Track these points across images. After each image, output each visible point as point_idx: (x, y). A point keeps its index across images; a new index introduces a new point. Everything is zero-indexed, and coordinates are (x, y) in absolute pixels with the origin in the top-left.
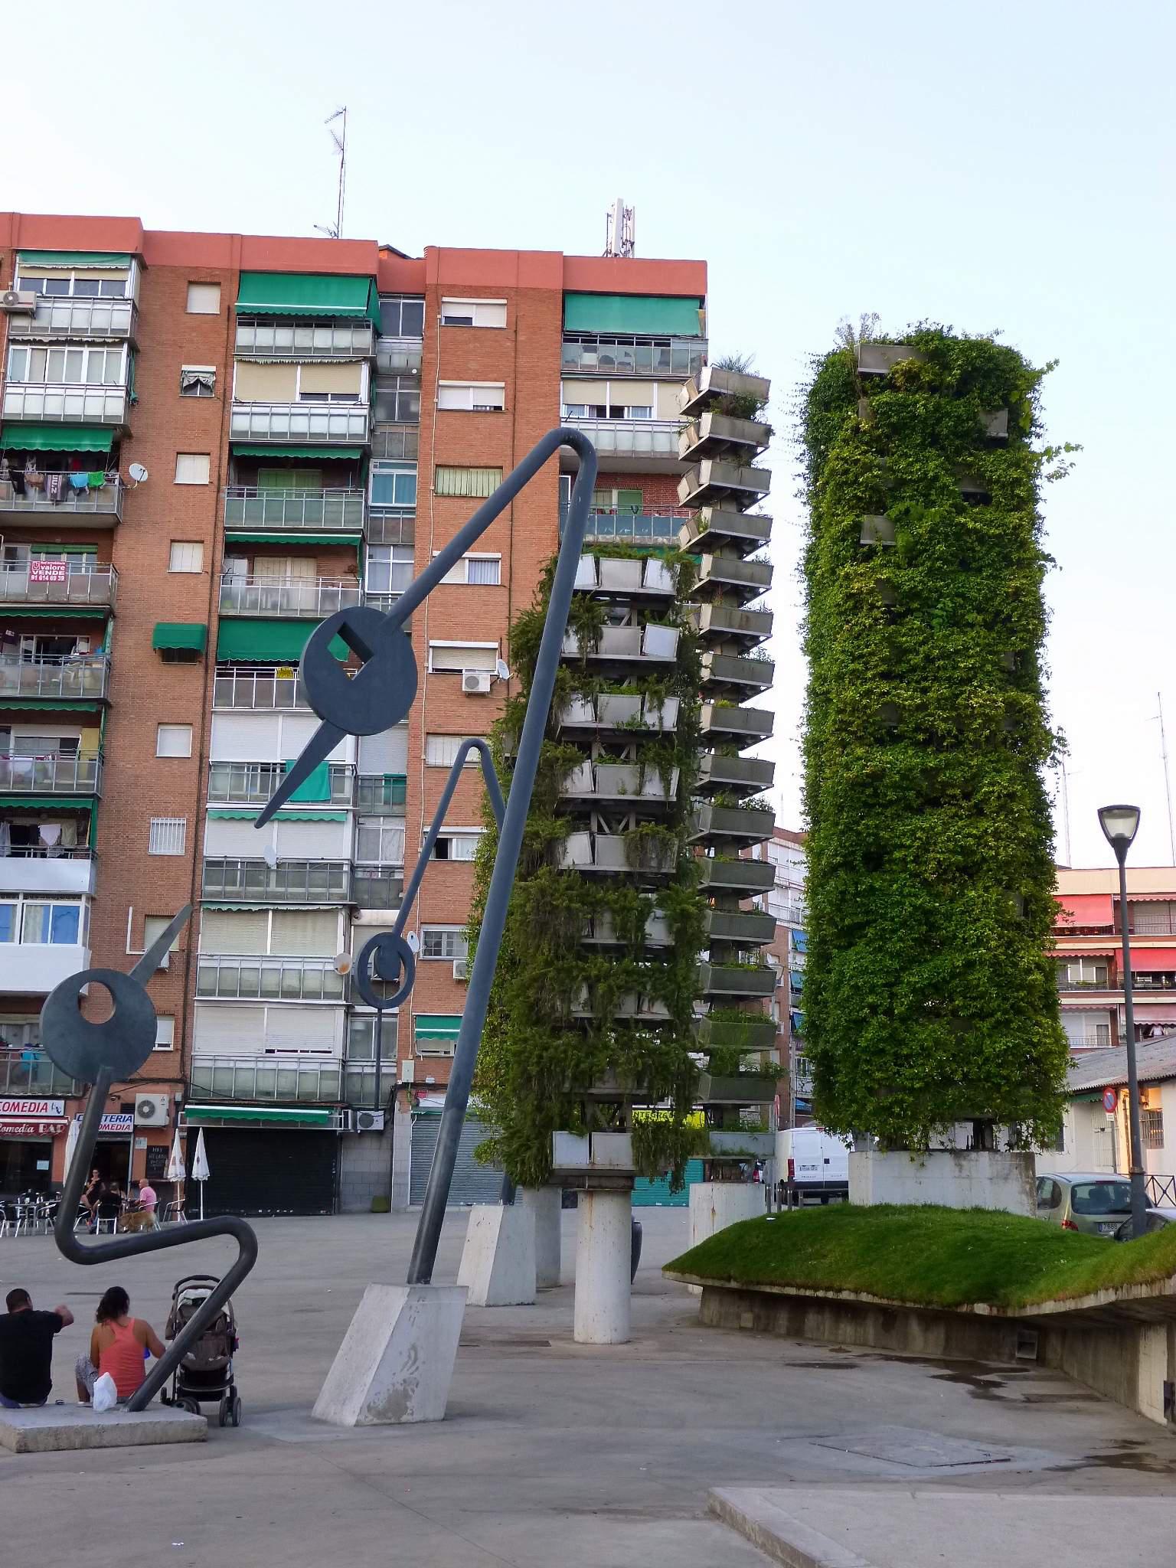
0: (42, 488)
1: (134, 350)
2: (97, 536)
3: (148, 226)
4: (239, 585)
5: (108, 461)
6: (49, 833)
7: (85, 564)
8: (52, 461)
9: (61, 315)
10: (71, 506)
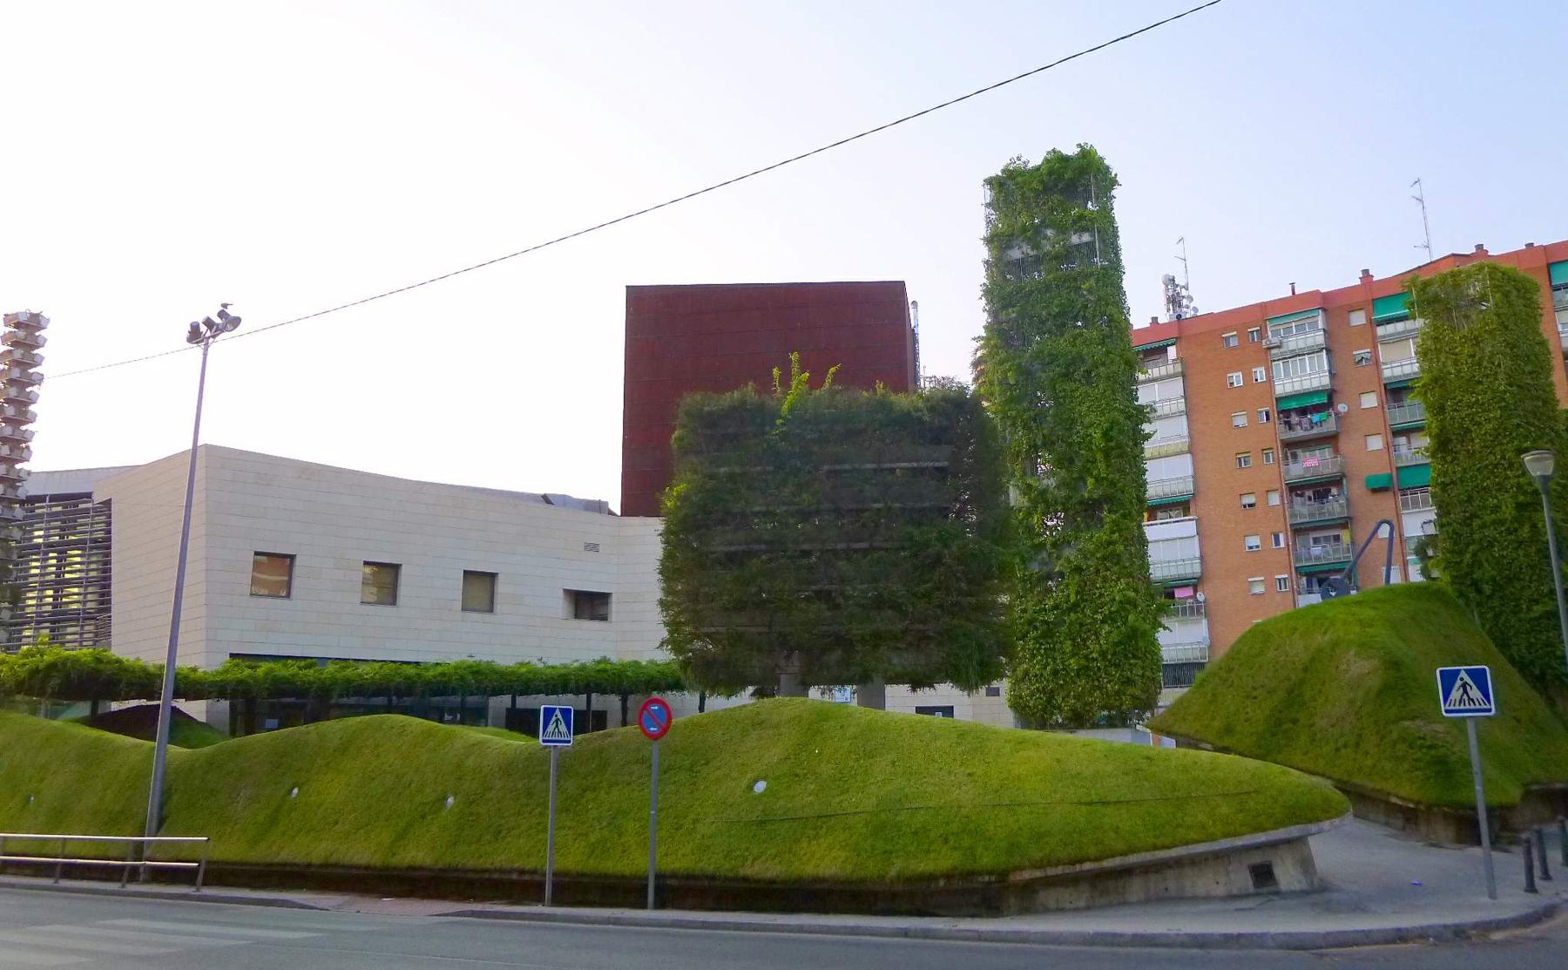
0: (1300, 423)
1: (1329, 351)
2: (1330, 440)
3: (1323, 290)
4: (1404, 450)
5: (1330, 404)
6: (447, 717)
7: (1327, 453)
8: (1303, 412)
9: (1293, 343)
10: (1315, 431)
